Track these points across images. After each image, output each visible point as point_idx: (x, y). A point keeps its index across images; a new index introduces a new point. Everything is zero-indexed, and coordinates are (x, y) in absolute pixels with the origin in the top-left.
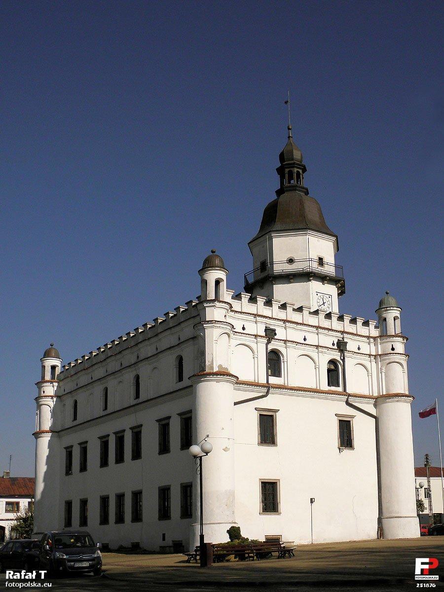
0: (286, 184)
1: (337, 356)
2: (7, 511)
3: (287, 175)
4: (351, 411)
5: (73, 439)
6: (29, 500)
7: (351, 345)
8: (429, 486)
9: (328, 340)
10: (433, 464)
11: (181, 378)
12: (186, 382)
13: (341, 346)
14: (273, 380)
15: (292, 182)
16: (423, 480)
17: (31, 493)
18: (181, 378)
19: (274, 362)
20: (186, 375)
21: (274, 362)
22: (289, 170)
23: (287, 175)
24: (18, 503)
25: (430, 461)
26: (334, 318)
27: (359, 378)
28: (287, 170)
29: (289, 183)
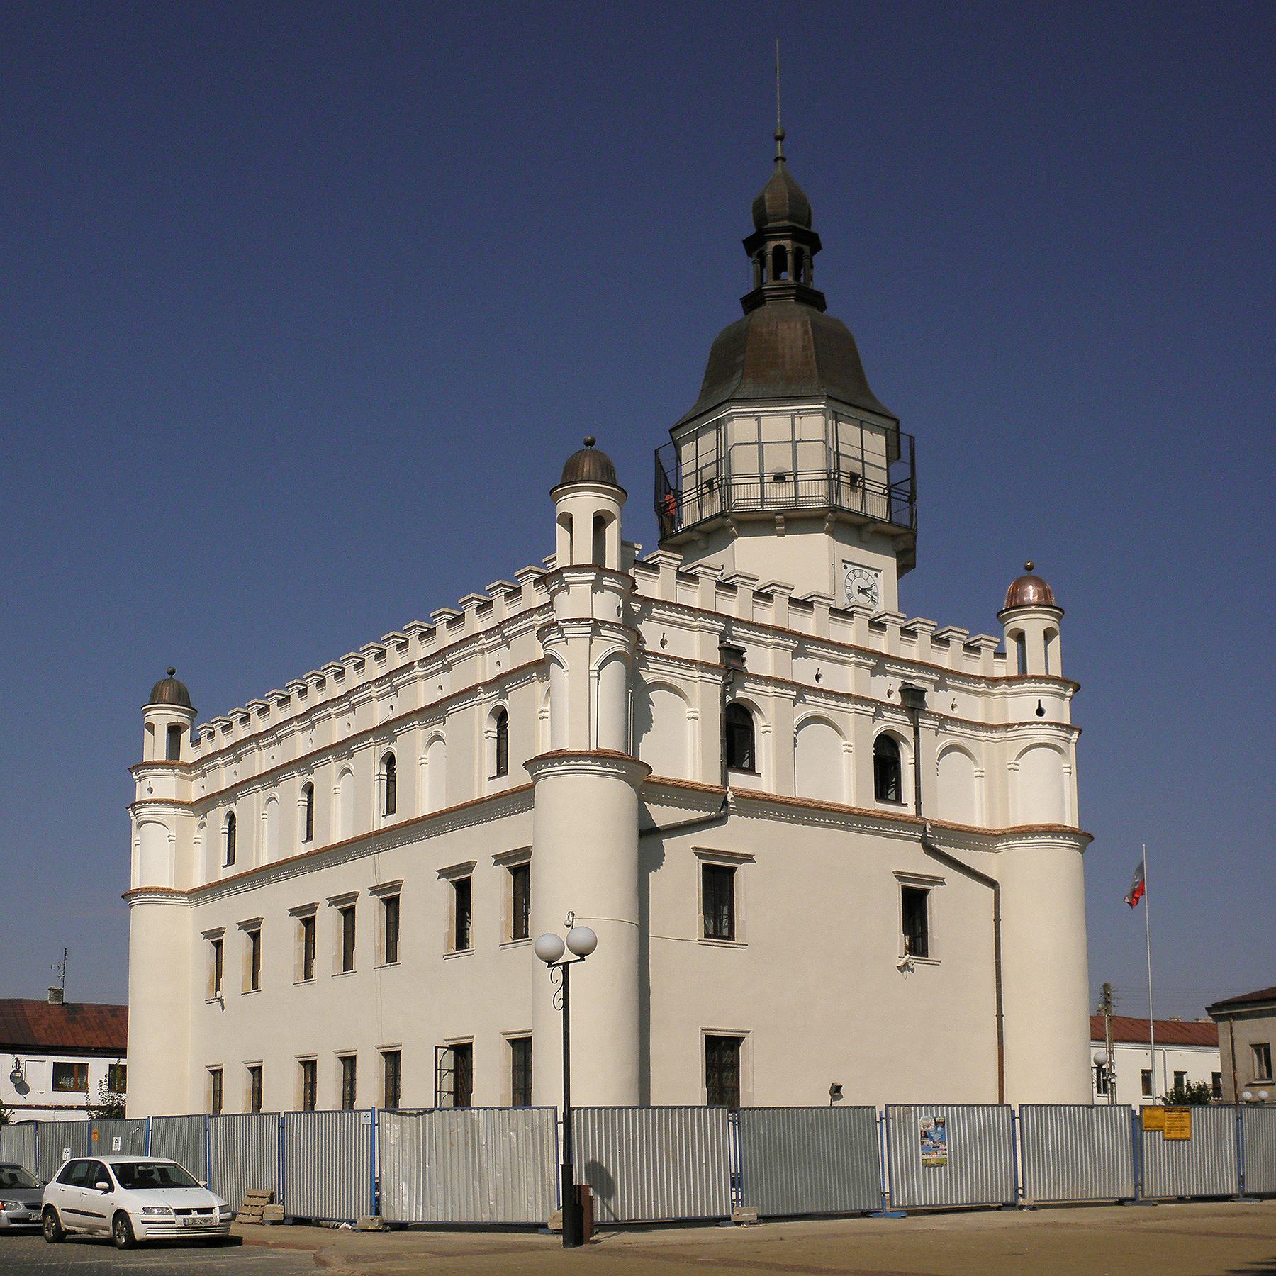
0: (769, 281)
1: (898, 723)
2: (57, 1086)
3: (769, 259)
4: (932, 867)
5: (229, 912)
6: (114, 1061)
7: (937, 701)
8: (1022, 1207)
9: (886, 688)
10: (1122, 1009)
11: (502, 770)
12: (517, 777)
13: (913, 700)
14: (738, 780)
15: (783, 275)
16: (1099, 1051)
17: (117, 1045)
18: (502, 770)
19: (737, 739)
20: (516, 758)
21: (737, 739)
22: (784, 246)
23: (769, 259)
24: (84, 1067)
25: (1113, 1002)
26: (893, 630)
27: (955, 789)
28: (772, 244)
29: (776, 277)
